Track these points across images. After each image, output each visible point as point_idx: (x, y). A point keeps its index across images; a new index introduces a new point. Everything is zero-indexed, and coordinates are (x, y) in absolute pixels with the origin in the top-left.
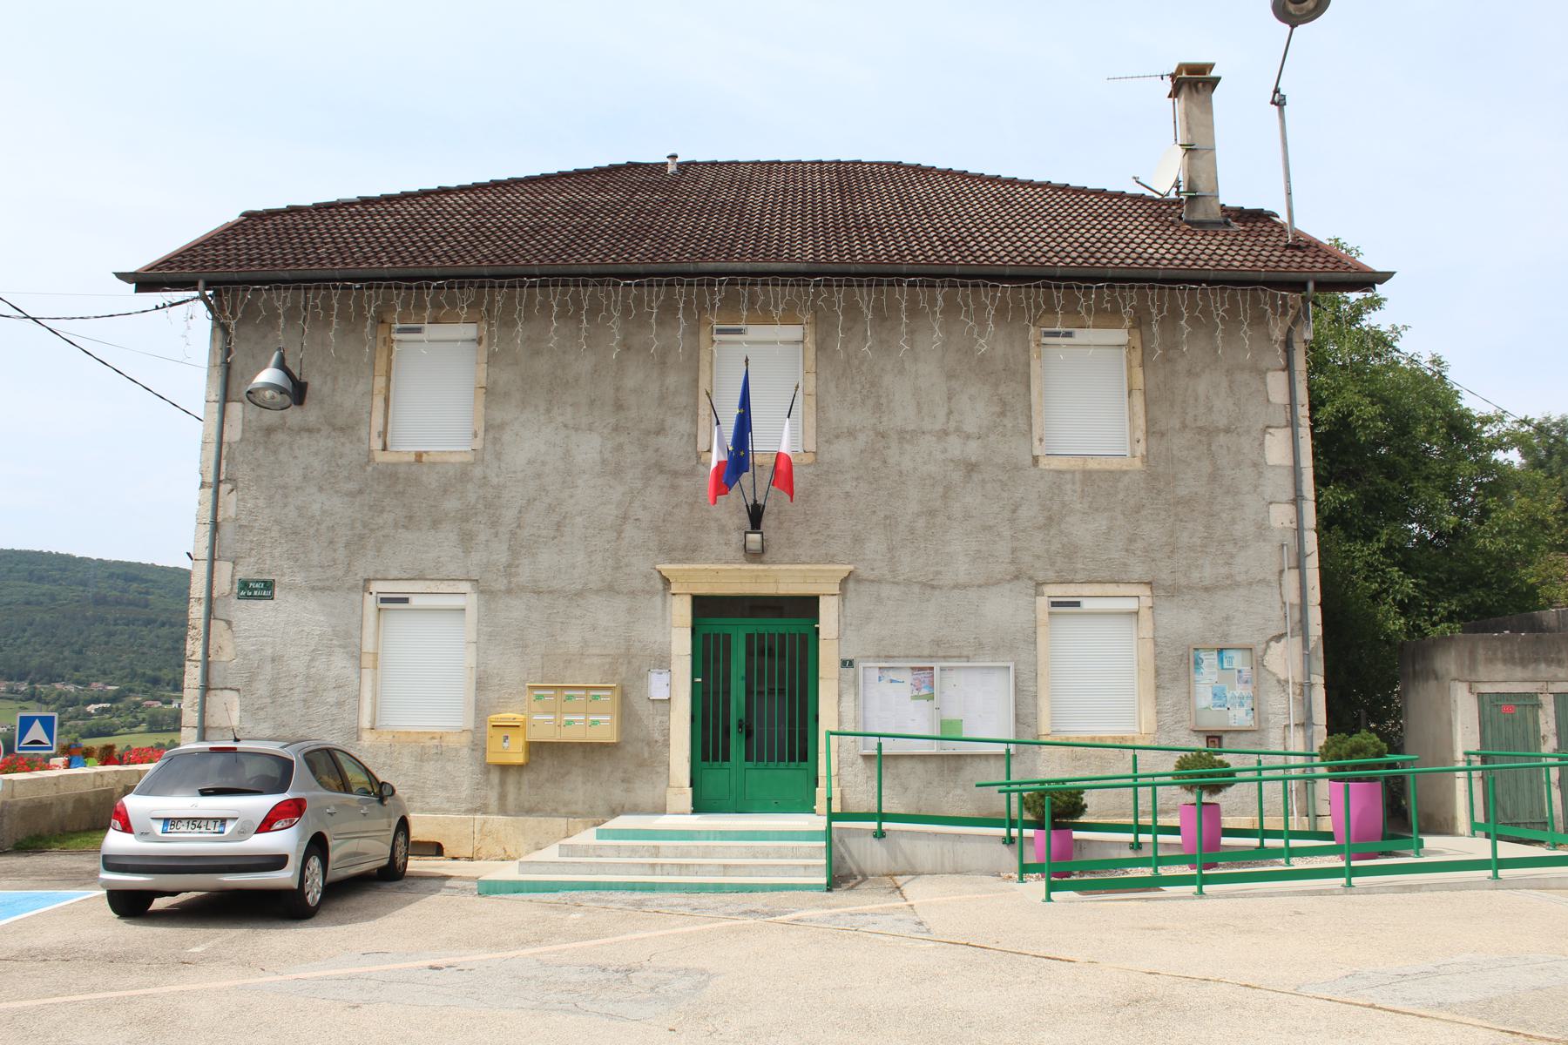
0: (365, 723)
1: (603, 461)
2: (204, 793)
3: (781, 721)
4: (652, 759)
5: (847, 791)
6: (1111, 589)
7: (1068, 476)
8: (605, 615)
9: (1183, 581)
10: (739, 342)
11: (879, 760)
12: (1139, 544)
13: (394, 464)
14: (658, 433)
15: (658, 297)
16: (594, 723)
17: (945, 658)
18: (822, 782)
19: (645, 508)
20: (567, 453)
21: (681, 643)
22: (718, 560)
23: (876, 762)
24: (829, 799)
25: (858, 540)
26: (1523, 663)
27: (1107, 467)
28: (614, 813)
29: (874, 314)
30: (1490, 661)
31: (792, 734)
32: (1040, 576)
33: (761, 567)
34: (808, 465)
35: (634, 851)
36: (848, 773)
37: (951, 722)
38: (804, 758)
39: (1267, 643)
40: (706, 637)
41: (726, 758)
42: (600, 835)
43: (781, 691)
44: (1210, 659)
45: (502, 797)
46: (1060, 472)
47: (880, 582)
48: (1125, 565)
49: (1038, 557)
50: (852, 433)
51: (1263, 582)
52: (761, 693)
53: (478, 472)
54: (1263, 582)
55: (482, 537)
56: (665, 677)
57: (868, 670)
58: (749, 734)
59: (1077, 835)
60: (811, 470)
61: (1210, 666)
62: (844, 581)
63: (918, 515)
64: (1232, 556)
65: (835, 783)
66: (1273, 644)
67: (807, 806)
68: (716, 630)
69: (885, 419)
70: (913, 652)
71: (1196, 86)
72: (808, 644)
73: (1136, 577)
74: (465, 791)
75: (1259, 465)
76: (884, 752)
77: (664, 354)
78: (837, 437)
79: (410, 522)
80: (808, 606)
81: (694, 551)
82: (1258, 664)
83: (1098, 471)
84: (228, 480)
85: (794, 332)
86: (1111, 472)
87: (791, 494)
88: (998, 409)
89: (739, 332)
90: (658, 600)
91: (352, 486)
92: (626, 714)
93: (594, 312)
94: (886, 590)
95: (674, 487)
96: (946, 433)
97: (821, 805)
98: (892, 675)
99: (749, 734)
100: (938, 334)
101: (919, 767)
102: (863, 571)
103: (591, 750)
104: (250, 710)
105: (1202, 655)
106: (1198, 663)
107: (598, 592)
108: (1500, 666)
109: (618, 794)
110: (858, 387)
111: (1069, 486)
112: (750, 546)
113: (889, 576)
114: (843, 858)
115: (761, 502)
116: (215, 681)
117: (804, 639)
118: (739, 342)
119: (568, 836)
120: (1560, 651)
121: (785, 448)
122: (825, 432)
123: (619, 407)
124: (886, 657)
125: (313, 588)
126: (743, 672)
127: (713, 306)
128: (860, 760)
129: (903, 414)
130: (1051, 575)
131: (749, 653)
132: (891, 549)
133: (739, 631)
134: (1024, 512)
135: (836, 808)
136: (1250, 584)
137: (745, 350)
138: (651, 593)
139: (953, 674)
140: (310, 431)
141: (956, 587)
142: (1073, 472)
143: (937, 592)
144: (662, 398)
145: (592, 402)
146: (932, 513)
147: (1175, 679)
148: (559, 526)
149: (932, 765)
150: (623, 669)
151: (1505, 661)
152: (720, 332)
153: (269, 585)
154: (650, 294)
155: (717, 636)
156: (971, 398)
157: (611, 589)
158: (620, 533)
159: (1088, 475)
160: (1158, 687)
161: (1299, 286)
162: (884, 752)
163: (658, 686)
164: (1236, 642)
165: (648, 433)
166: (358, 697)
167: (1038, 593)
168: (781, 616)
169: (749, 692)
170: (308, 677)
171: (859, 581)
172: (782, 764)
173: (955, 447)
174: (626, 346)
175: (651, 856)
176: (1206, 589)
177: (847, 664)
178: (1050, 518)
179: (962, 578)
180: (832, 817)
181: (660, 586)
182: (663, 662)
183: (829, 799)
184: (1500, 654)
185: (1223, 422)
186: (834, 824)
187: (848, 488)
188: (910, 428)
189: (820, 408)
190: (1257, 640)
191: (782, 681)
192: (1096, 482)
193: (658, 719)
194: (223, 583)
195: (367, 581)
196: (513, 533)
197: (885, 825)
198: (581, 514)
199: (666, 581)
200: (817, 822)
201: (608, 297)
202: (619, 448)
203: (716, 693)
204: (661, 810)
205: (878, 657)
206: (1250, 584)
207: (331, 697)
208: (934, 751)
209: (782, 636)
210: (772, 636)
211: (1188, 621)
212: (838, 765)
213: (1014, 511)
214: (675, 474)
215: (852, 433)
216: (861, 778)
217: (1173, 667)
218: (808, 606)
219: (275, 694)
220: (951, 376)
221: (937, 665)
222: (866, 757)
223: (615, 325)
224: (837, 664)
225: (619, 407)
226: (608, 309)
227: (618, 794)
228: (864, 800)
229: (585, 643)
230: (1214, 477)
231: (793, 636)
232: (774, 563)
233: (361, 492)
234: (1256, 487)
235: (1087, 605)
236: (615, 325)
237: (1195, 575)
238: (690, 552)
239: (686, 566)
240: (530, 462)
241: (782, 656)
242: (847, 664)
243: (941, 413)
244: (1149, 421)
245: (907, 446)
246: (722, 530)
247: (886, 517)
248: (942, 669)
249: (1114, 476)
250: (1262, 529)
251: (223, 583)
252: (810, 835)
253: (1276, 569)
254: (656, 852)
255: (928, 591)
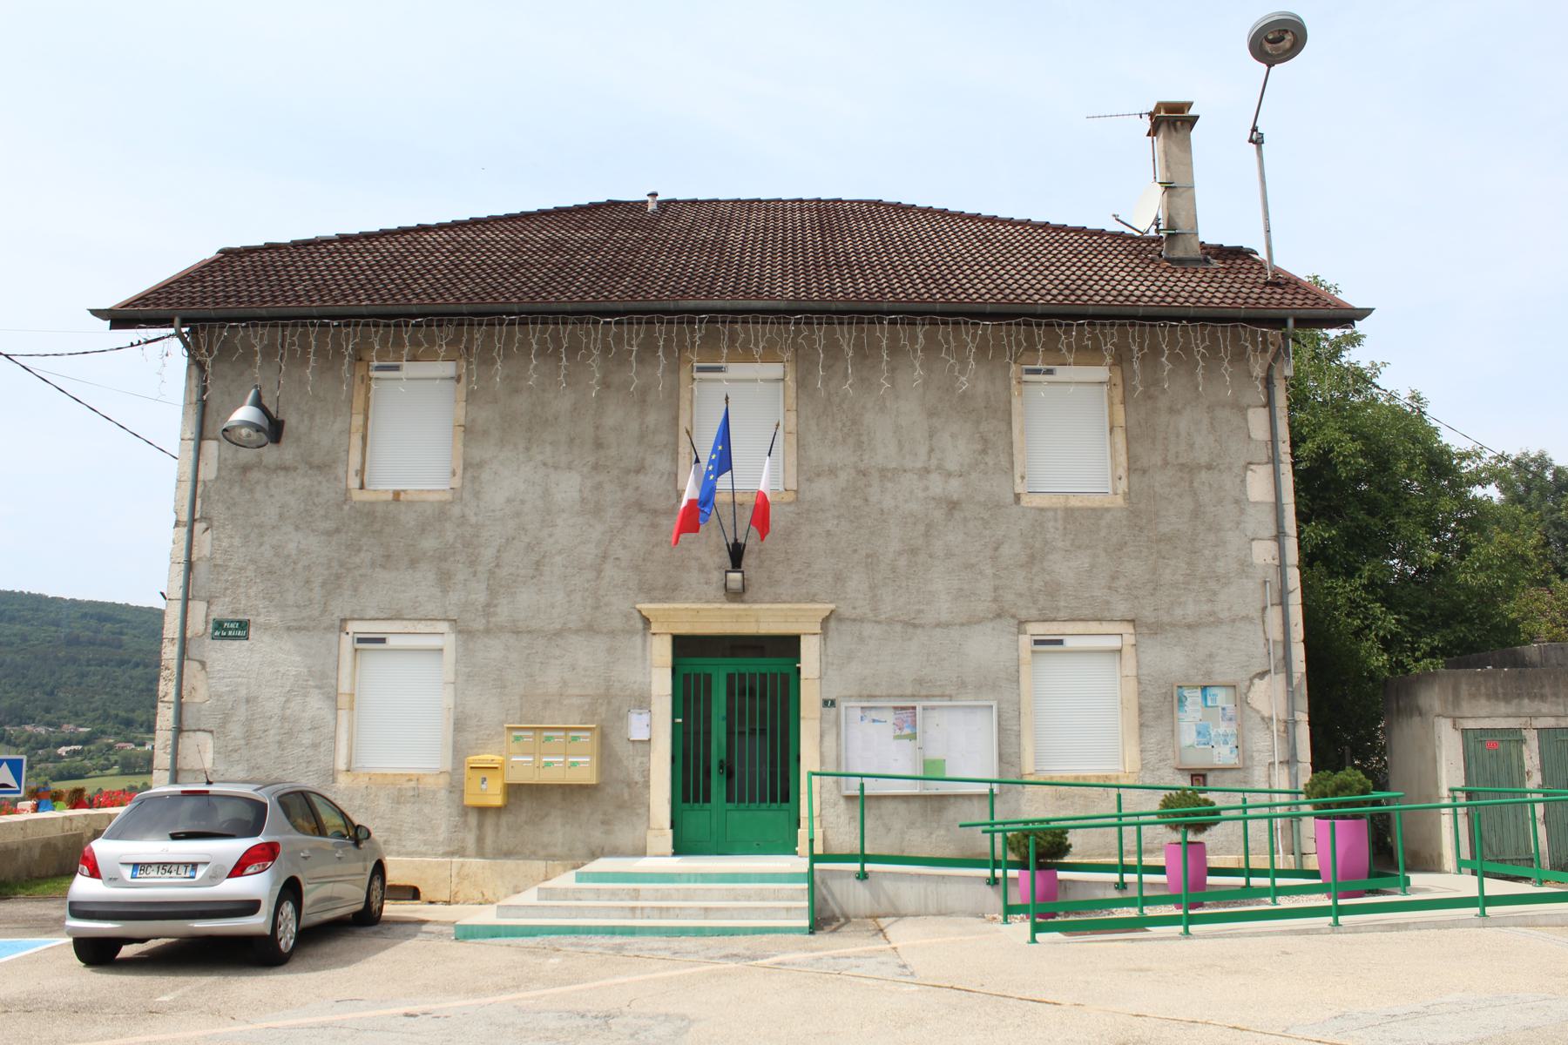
0: (341, 764)
1: (583, 500)
2: (175, 837)
3: (763, 762)
4: (633, 802)
5: (829, 833)
6: (1094, 627)
7: (1050, 514)
8: (585, 655)
9: (1166, 619)
10: (719, 380)
11: (862, 801)
12: (1122, 582)
13: (372, 503)
14: (638, 472)
15: (638, 335)
16: (573, 764)
17: (928, 697)
18: (804, 823)
19: (625, 547)
20: (546, 493)
21: (661, 684)
22: (699, 600)
23: (859, 802)
24: (812, 841)
25: (839, 578)
26: (1507, 698)
27: (1089, 505)
28: (593, 856)
29: (855, 353)
30: (1473, 696)
31: (773, 775)
32: (1023, 614)
33: (742, 606)
34: (789, 504)
35: (614, 894)
36: (830, 815)
37: (933, 762)
38: (786, 798)
39: (1251, 680)
40: (686, 677)
41: (707, 799)
42: (580, 878)
43: (763, 731)
44: (1193, 697)
45: (480, 840)
46: (1042, 510)
47: (862, 620)
48: (1108, 602)
49: (1021, 595)
50: (832, 472)
51: (1246, 618)
52: (742, 733)
53: (456, 511)
54: (1247, 618)
55: (460, 577)
56: (645, 717)
57: (850, 710)
58: (730, 775)
59: (1061, 875)
60: (792, 508)
61: (1194, 703)
62: (826, 621)
63: (900, 554)
64: (1215, 593)
65: (816, 823)
66: (1256, 681)
67: (789, 848)
68: (698, 670)
69: (866, 457)
70: (896, 692)
71: (1174, 123)
72: (788, 685)
73: (1118, 615)
74: (442, 833)
75: (1241, 502)
76: (867, 792)
77: (644, 392)
78: (819, 475)
79: (387, 561)
80: (788, 646)
81: (674, 590)
82: (1242, 701)
83: (1079, 509)
84: (203, 518)
85: (775, 370)
86: (1094, 510)
87: (763, 538)
88: (979, 447)
89: (719, 369)
90: (638, 640)
91: (329, 525)
92: (606, 755)
93: (573, 350)
94: (868, 629)
95: (654, 526)
96: (927, 471)
97: (803, 846)
98: (874, 714)
99: (730, 775)
100: (919, 372)
101: (902, 807)
102: (845, 610)
103: (571, 792)
104: (224, 753)
105: (1186, 693)
106: (1181, 701)
107: (577, 632)
108: (1483, 701)
109: (597, 836)
110: (839, 425)
111: (1051, 524)
112: (731, 585)
113: (870, 615)
114: (825, 900)
115: (741, 540)
116: (188, 722)
117: (785, 679)
118: (719, 380)
119: (547, 879)
120: (1542, 687)
121: (763, 486)
122: (806, 471)
123: (599, 445)
124: (868, 697)
125: (288, 629)
126: (724, 712)
127: (693, 343)
128: (842, 801)
129: (884, 452)
130: (1034, 612)
131: (730, 694)
132: (872, 588)
133: (720, 671)
134: (1006, 550)
135: (818, 850)
136: (1233, 621)
137: (725, 388)
138: (631, 632)
139: (936, 714)
140: (286, 469)
141: (938, 625)
142: (1055, 510)
143: (919, 631)
144: (641, 438)
145: (572, 440)
146: (914, 551)
147: (1159, 717)
148: (538, 564)
149: (915, 806)
150: (602, 710)
151: (1488, 697)
152: (700, 370)
153: (244, 625)
154: (630, 333)
155: (697, 676)
156: (953, 436)
157: (590, 629)
158: (599, 572)
159: (1070, 513)
160: (1141, 725)
161: (1279, 323)
162: (867, 792)
163: (637, 727)
164: (1220, 680)
165: (628, 472)
166: (334, 738)
167: (1021, 632)
168: (763, 655)
169: (730, 733)
170: (283, 719)
171: (840, 620)
172: (764, 806)
173: (936, 485)
174: (605, 384)
175: (632, 899)
176: (1189, 626)
177: (828, 703)
178: (1032, 557)
179: (945, 617)
180: (815, 858)
181: (640, 625)
182: (643, 702)
183: (812, 841)
184: (1483, 690)
185: (1204, 459)
186: (817, 866)
187: (829, 526)
188: (894, 465)
189: (800, 446)
190: (1241, 677)
191: (763, 721)
192: (1078, 520)
193: (638, 760)
194: (197, 623)
195: (344, 621)
196: (491, 572)
197: (868, 867)
198: (560, 553)
199: (647, 621)
200: (799, 864)
201: (588, 335)
202: (598, 487)
203: (697, 733)
204: (641, 852)
205: (860, 697)
206: (1233, 621)
207: (307, 738)
208: (916, 791)
209: (763, 676)
210: (753, 676)
211: (1172, 659)
212: (820, 808)
213: (996, 549)
214: (655, 512)
215: (832, 472)
216: (844, 819)
217: (1157, 705)
218: (788, 646)
219: (248, 736)
220: (932, 414)
221: (919, 705)
222: (849, 798)
223: (595, 363)
224: (819, 703)
225: (599, 445)
226: (587, 347)
227: (597, 836)
228: (846, 840)
229: (565, 683)
230: (1196, 514)
231: (774, 676)
232: (755, 602)
233: (337, 531)
234: (1238, 523)
235: (1070, 643)
236: (595, 363)
237: (1178, 612)
238: (671, 591)
239: (666, 606)
240: (509, 501)
241: (763, 695)
242: (828, 703)
243: (923, 450)
244: (1132, 458)
245: (889, 485)
246: (703, 569)
247: (868, 556)
248: (925, 709)
249: (1097, 513)
250: (1245, 566)
251: (197, 623)
252: (793, 877)
253: (1259, 606)
254: (636, 895)
255: (910, 630)
